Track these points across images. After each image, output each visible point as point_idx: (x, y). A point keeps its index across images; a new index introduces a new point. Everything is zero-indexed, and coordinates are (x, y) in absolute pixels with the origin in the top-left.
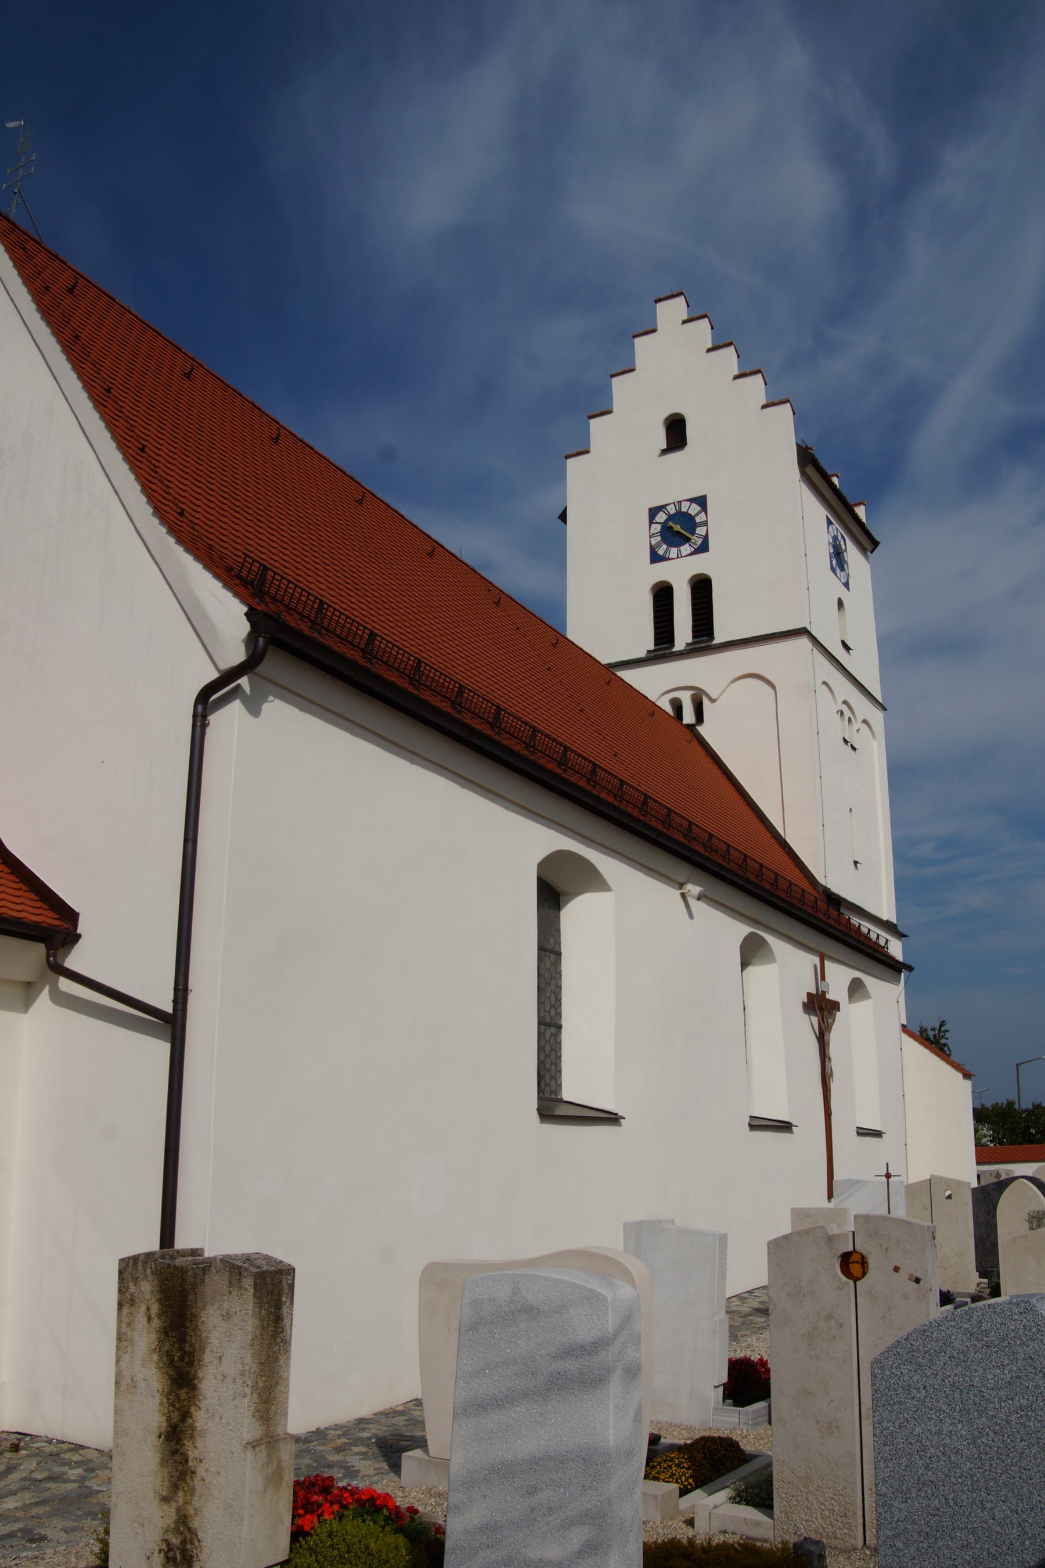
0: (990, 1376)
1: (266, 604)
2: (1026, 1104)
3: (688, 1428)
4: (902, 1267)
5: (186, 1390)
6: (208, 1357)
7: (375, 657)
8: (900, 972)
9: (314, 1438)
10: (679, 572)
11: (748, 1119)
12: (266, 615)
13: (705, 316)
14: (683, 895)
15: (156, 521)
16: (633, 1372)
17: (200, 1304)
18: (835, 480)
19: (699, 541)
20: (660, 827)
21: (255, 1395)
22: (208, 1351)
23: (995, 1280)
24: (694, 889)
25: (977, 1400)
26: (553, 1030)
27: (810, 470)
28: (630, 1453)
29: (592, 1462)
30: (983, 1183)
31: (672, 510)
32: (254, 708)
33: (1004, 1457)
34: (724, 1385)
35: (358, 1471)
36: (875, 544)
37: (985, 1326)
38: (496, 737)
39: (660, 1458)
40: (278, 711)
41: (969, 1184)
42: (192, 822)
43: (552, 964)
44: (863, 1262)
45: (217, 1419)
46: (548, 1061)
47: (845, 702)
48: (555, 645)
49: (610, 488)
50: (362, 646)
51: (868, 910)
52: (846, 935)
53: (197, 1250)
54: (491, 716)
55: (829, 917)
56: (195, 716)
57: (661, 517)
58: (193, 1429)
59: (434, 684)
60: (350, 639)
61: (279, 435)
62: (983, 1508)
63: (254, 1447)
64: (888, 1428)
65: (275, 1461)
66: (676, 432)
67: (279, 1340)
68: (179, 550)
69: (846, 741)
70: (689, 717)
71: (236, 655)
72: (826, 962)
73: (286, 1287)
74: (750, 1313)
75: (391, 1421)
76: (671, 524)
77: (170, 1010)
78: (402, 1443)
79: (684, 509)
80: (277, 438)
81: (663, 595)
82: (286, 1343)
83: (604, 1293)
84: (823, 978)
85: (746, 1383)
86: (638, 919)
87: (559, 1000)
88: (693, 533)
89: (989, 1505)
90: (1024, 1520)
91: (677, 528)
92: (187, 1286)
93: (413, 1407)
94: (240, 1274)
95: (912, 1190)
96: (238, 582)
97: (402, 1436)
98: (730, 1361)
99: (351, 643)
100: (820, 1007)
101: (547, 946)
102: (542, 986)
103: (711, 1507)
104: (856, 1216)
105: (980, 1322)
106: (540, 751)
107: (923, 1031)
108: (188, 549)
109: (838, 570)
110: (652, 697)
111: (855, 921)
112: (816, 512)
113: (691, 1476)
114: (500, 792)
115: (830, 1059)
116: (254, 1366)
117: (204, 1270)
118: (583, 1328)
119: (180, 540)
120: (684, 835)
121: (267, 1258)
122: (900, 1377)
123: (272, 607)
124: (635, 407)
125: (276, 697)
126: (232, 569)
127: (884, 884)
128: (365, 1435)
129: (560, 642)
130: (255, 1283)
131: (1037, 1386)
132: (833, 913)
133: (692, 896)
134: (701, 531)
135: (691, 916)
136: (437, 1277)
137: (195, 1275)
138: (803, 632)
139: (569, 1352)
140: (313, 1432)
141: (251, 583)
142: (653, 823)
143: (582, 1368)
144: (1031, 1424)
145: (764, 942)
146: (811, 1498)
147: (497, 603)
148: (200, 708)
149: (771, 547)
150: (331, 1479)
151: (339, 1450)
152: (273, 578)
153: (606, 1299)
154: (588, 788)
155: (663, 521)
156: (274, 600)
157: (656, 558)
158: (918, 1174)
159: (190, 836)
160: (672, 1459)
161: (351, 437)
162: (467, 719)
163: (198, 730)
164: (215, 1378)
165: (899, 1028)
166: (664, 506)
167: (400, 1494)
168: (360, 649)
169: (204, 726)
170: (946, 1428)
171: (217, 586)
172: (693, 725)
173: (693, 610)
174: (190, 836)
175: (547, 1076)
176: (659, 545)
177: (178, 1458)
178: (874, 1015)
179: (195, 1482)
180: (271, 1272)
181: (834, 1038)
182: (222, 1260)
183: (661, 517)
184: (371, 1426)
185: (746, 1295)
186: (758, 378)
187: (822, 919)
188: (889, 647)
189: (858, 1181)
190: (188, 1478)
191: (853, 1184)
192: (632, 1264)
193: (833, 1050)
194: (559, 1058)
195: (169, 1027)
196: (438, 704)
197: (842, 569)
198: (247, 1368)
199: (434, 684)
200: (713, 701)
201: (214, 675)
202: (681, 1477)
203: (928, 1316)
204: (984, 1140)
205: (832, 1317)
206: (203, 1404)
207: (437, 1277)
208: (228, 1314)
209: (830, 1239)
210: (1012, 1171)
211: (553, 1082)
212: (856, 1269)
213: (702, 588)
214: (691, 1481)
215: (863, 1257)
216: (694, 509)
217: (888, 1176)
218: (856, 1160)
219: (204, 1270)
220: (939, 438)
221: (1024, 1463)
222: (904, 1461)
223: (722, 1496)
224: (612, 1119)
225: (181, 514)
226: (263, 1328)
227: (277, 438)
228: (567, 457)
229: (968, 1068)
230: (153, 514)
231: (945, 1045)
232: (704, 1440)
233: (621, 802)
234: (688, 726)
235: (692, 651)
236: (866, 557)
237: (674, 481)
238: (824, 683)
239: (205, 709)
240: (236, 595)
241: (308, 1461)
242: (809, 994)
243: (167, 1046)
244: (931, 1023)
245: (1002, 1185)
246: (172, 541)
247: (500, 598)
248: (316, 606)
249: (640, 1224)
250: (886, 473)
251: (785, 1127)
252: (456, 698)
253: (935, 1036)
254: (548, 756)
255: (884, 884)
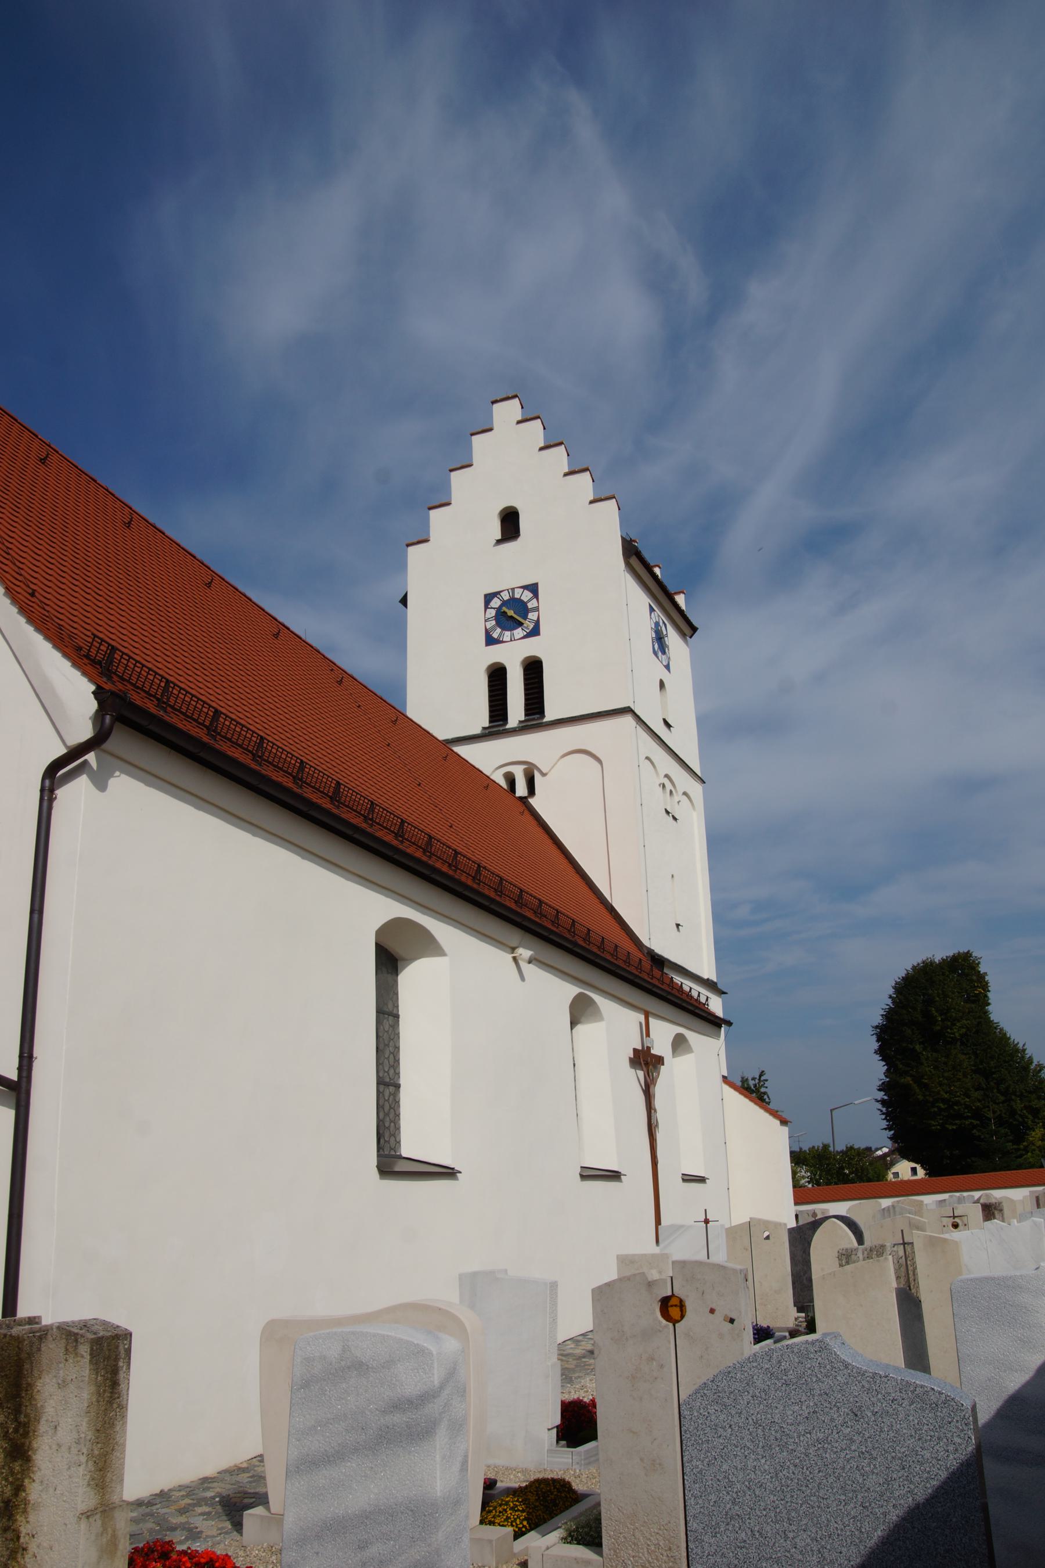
0: (789, 1413)
1: (113, 683)
2: (840, 1146)
3: (524, 1471)
4: (717, 1309)
5: (20, 1462)
6: (43, 1427)
7: (219, 734)
8: (720, 1027)
9: (158, 1501)
10: (512, 654)
11: (579, 1170)
12: (113, 693)
13: (538, 417)
14: (515, 959)
15: (7, 601)
16: (458, 1427)
17: (36, 1373)
18: (657, 571)
19: (531, 626)
20: (492, 895)
21: (90, 1463)
22: (43, 1421)
23: (810, 1314)
24: (524, 953)
25: (778, 1436)
26: (392, 1089)
27: (634, 560)
28: (457, 1502)
29: (421, 1514)
30: (801, 1223)
31: (506, 596)
32: (100, 783)
33: (804, 1488)
34: (557, 1427)
35: (201, 1532)
36: (694, 629)
37: (784, 1365)
38: (335, 811)
39: (494, 1500)
40: (124, 786)
41: (785, 1225)
42: (38, 893)
43: (391, 1026)
44: (682, 1306)
45: (51, 1490)
46: (388, 1119)
47: (667, 776)
48: (394, 722)
49: (448, 576)
50: (207, 723)
51: (689, 969)
52: (669, 993)
53: (35, 1318)
54: (332, 790)
55: (653, 977)
56: (42, 790)
57: (496, 603)
58: (26, 1502)
59: (276, 760)
60: (195, 716)
61: (132, 519)
62: (786, 1538)
63: (88, 1517)
64: (697, 1467)
65: (110, 1531)
66: (510, 524)
67: (115, 1406)
68: (30, 629)
69: (668, 812)
70: (521, 790)
71: (84, 732)
72: (651, 1019)
73: (122, 1352)
74: (576, 1358)
75: (235, 1478)
76: (504, 609)
77: (15, 1078)
78: (246, 1501)
79: (517, 596)
80: (129, 523)
81: (497, 676)
82: (123, 1408)
83: (430, 1347)
84: (648, 1035)
85: (577, 1424)
86: (473, 985)
87: (397, 1061)
88: (525, 617)
89: (791, 1535)
90: (823, 1547)
91: (511, 613)
92: (23, 1355)
93: (257, 1463)
94: (76, 1341)
95: (732, 1233)
96: (86, 661)
97: (246, 1493)
98: (563, 1403)
99: (196, 721)
100: (646, 1061)
101: (385, 1009)
102: (381, 1046)
103: (544, 1548)
104: (673, 1262)
105: (779, 1362)
106: (378, 824)
107: (744, 1081)
108: (39, 629)
109: (660, 654)
110: (487, 771)
111: (678, 979)
112: (639, 600)
113: (525, 1519)
114: (338, 863)
115: (655, 1111)
116: (90, 1433)
117: (40, 1338)
118: (410, 1382)
119: (31, 620)
120: (516, 902)
121: (105, 1323)
122: (697, 1421)
123: (120, 686)
124: (473, 499)
125: (122, 772)
126: (81, 648)
127: (704, 944)
128: (209, 1494)
129: (399, 718)
130: (92, 1349)
131: (832, 1420)
132: (656, 973)
133: (523, 960)
134: (533, 616)
135: (523, 979)
136: (277, 1334)
137: (31, 1344)
138: (628, 710)
139: (398, 1406)
140: (156, 1495)
141: (100, 663)
142: (486, 892)
143: (410, 1421)
144: (827, 1456)
145: (591, 1002)
146: (637, 1534)
147: (340, 682)
148: (47, 783)
149: (599, 633)
150: (170, 1543)
151: (182, 1511)
152: (122, 657)
153: (431, 1353)
154: (424, 858)
155: (497, 606)
156: (122, 678)
157: (490, 641)
158: (740, 1217)
159: (37, 907)
160: (507, 1503)
161: (205, 526)
162: (308, 794)
163: (45, 804)
164: (50, 1447)
165: (720, 1079)
166: (499, 593)
167: (241, 1553)
168: (205, 726)
169: (51, 800)
170: (750, 1464)
171: (66, 664)
172: (525, 798)
173: (526, 690)
174: (37, 907)
175: (387, 1135)
176: (493, 629)
177: (9, 1535)
178: (697, 1068)
179: (27, 1560)
180: (107, 1338)
181: (660, 1090)
182: (58, 1328)
183: (496, 603)
184: (215, 1484)
185: (580, 1338)
186: (586, 476)
187: (649, 979)
188: (713, 728)
189: (682, 1226)
190: (19, 1555)
191: (677, 1228)
192: (466, 1316)
193: (658, 1103)
194: (398, 1115)
195: (14, 1094)
196: (280, 779)
197: (664, 653)
198: (83, 1435)
199: (276, 760)
200: (544, 775)
201: (62, 751)
202: (515, 1519)
203: (742, 1354)
204: (803, 1181)
205: (653, 1359)
206: (37, 1477)
207: (277, 1334)
208: (64, 1381)
209: (650, 1285)
210: (827, 1210)
211: (392, 1139)
212: (674, 1312)
213: (533, 669)
214: (525, 1523)
215: (681, 1301)
216: (527, 596)
217: (707, 1221)
218: (681, 1206)
219: (40, 1338)
220: (744, 538)
221: (822, 1493)
222: (713, 1498)
223: (555, 1536)
224: (449, 1173)
225: (33, 595)
226: (99, 1394)
227: (129, 523)
228: (408, 545)
229: (784, 1115)
230: (5, 594)
231: (765, 1093)
232: (538, 1481)
233: (455, 871)
234: (521, 798)
235: (524, 728)
236: (686, 642)
237: (508, 569)
238: (647, 758)
239: (52, 783)
240: (85, 673)
241: (150, 1525)
242: (635, 1050)
243: (12, 1113)
244: (752, 1073)
245: (816, 1224)
246: (22, 620)
247: (342, 678)
248: (163, 684)
249: (475, 1275)
250: (700, 568)
251: (614, 1176)
252: (298, 773)
253: (755, 1086)
254: (386, 828)
255: (704, 944)
